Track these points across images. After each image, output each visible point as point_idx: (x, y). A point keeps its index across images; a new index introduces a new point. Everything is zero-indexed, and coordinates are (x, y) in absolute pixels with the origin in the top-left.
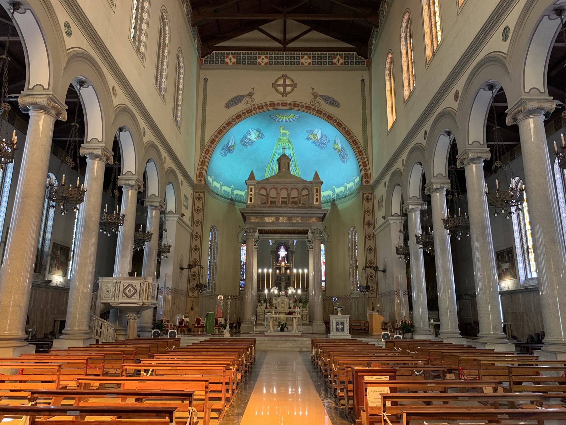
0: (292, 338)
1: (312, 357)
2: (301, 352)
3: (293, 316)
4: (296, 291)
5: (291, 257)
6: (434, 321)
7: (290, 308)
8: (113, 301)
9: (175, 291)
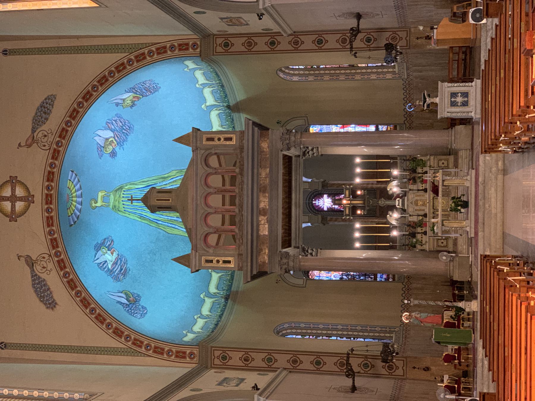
0: (481, 187)
1: (515, 152)
2: (505, 172)
3: (441, 184)
7: (425, 190)
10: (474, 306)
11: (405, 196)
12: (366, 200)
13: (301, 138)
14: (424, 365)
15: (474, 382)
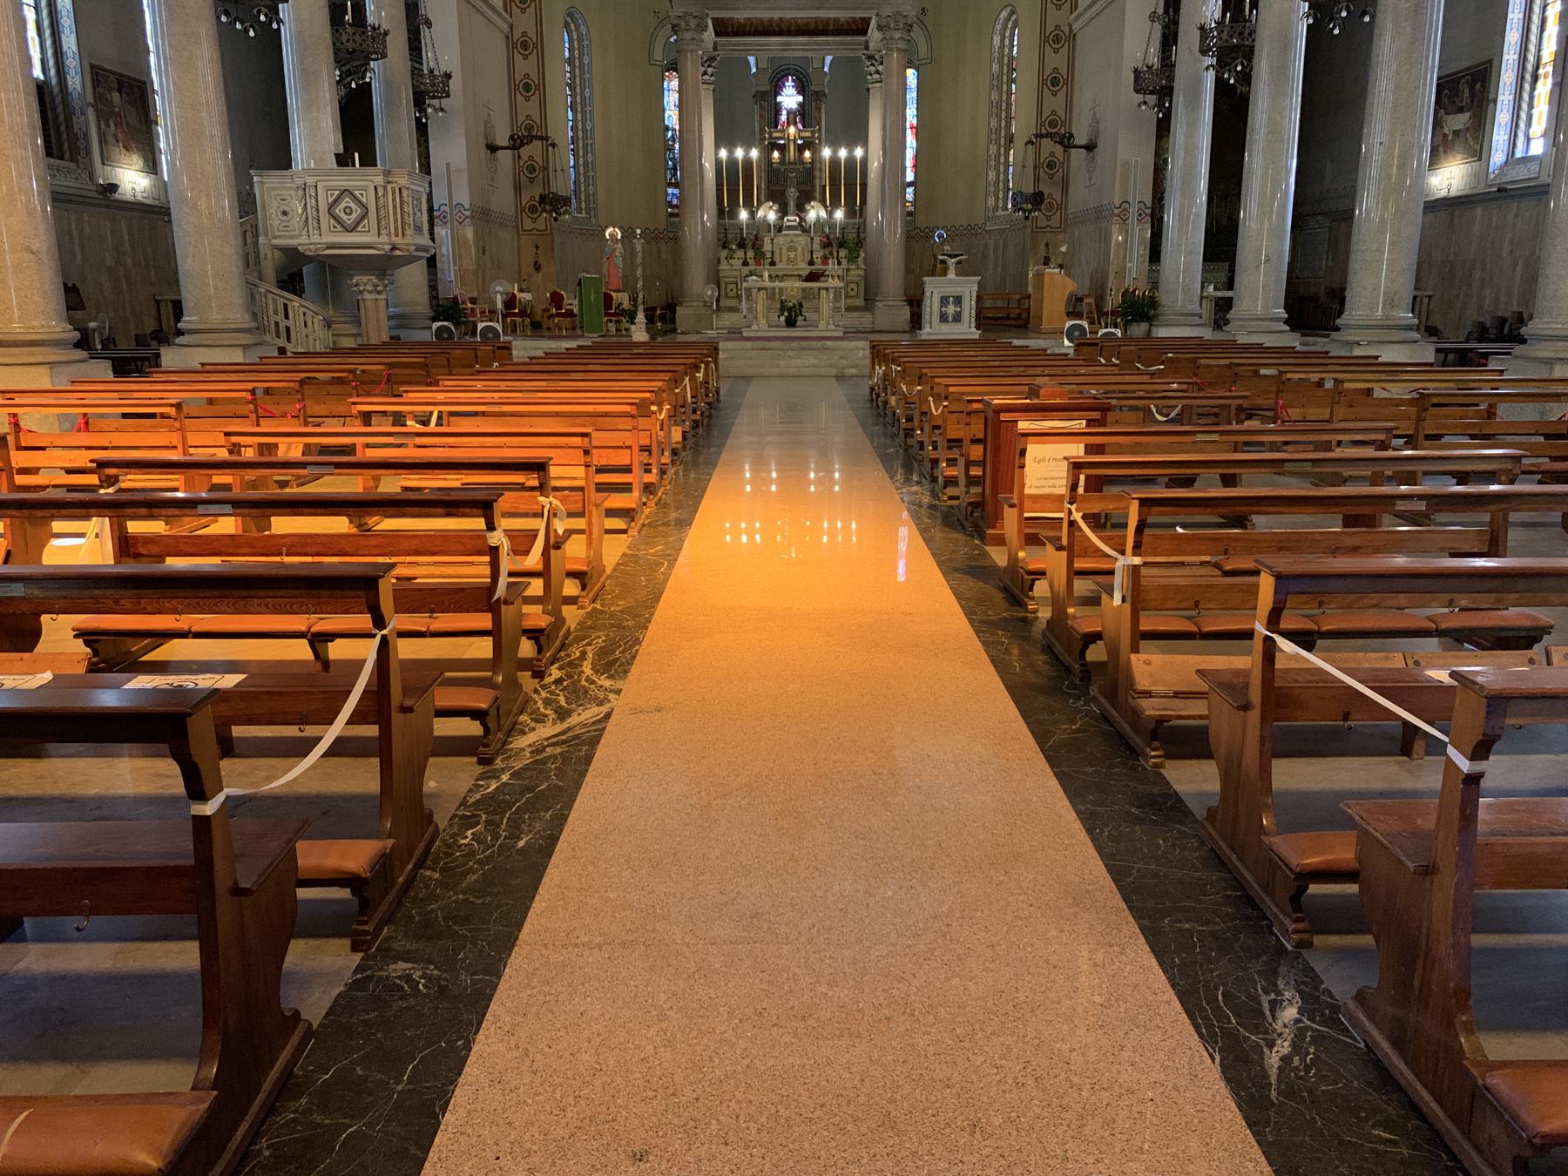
0: (818, 344)
1: (872, 389)
2: (841, 378)
3: (822, 285)
4: (830, 214)
5: (815, 114)
6: (1216, 289)
7: (811, 263)
8: (304, 239)
9: (483, 216)
10: (639, 334)
11: (803, 231)
12: (796, 167)
13: (898, 50)
14: (544, 263)
15: (525, 337)
